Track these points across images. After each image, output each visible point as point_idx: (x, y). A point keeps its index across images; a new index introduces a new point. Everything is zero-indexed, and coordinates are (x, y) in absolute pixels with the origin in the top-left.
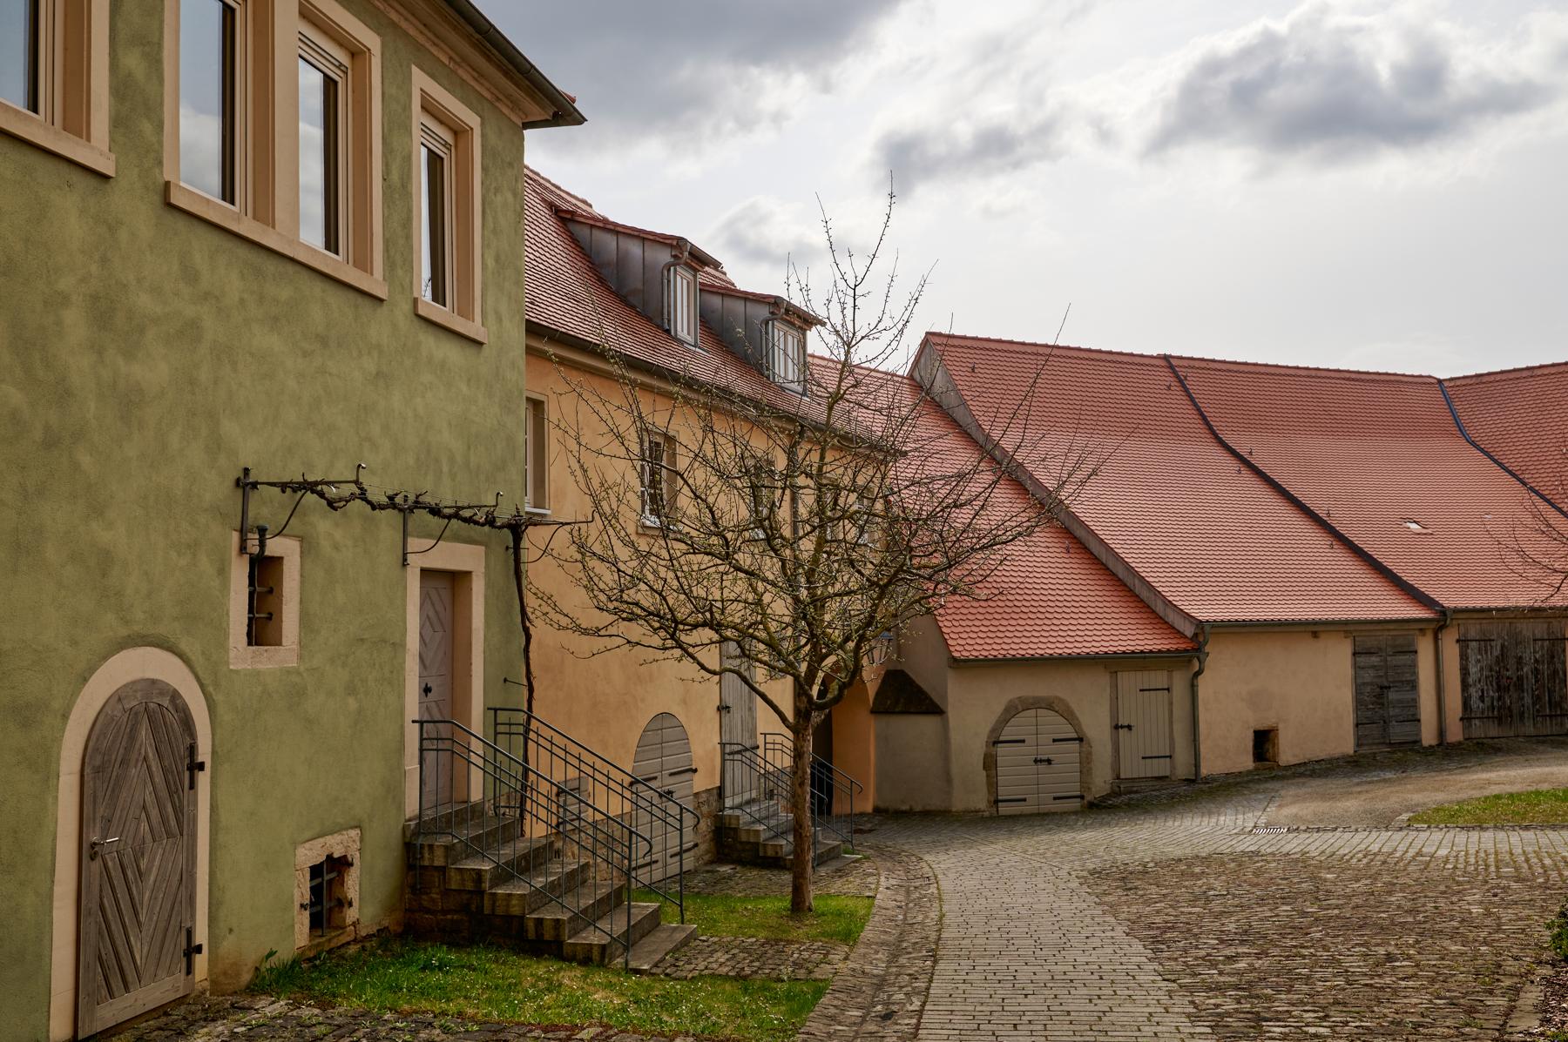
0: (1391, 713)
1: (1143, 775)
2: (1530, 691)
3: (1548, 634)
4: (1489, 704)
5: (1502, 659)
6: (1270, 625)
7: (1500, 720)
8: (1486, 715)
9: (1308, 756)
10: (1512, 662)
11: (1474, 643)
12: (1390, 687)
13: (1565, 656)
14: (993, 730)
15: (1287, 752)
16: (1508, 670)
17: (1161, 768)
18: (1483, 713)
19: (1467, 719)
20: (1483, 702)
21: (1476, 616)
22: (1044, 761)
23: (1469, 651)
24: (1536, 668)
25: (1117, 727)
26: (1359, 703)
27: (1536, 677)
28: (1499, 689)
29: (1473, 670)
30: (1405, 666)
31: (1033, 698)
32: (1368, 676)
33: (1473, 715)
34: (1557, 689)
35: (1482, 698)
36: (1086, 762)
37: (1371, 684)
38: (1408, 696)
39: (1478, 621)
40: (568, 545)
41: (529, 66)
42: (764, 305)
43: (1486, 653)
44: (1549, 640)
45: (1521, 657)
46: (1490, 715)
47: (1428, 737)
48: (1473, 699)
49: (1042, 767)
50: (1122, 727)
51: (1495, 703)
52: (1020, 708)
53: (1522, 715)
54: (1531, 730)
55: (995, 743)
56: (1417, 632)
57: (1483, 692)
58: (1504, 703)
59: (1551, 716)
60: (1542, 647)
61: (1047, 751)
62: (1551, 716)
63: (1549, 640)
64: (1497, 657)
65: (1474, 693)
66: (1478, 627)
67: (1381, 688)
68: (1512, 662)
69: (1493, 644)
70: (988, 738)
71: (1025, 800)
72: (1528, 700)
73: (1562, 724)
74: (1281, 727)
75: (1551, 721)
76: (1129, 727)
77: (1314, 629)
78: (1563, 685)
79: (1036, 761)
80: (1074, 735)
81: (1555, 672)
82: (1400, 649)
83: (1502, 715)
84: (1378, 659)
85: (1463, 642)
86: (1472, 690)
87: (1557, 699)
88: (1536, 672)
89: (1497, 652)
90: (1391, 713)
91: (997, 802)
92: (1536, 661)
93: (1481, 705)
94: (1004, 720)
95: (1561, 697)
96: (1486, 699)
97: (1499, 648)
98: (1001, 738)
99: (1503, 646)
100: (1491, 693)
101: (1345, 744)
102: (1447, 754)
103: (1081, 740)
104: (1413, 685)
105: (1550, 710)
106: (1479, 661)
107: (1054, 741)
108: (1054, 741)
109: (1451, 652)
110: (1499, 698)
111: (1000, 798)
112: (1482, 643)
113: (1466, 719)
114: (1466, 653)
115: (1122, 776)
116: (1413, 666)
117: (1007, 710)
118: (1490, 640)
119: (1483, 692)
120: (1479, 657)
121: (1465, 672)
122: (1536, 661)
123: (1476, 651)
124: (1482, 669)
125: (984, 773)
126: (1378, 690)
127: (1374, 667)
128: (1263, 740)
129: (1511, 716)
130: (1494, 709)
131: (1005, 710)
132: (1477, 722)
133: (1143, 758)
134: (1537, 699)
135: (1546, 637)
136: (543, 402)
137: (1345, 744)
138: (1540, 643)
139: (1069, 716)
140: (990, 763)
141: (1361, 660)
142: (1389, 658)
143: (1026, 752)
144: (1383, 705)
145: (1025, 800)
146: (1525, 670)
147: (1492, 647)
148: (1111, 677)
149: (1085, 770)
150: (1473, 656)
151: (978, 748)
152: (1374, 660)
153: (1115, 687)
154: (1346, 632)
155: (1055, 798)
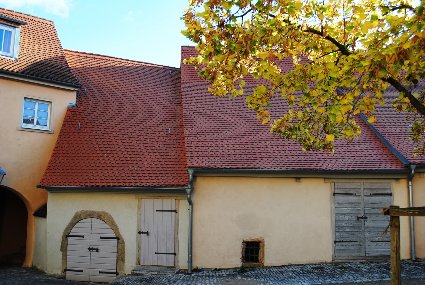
1: (152, 265)
14: (67, 229)
17: (167, 261)
22: (94, 249)
25: (140, 233)
40: (338, 116)
42: (415, 220)
49: (94, 253)
50: (143, 233)
52: (82, 217)
61: (97, 243)
70: (64, 233)
71: (82, 271)
76: (147, 233)
79: (90, 249)
82: (375, 192)
91: (66, 270)
94: (72, 224)
103: (118, 239)
107: (101, 238)
108: (101, 238)
111: (68, 268)
115: (142, 263)
117: (75, 218)
125: (61, 253)
131: (74, 217)
139: (113, 225)
140: (64, 248)
143: (86, 243)
145: (82, 271)
148: (138, 201)
149: (120, 257)
151: (59, 237)
153: (139, 208)
155: (100, 272)
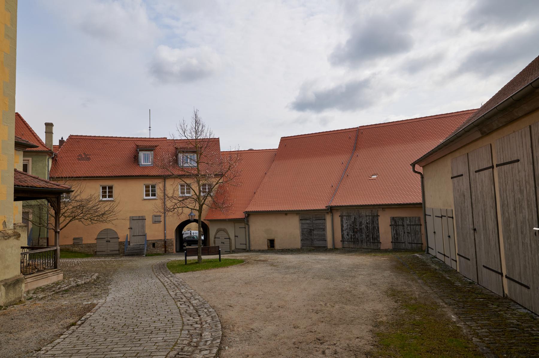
0: (314, 238)
2: (365, 233)
3: (371, 214)
4: (350, 237)
5: (354, 222)
6: (269, 212)
7: (354, 242)
8: (349, 240)
9: (284, 248)
10: (358, 224)
11: (345, 217)
12: (314, 230)
13: (378, 222)
15: (277, 246)
16: (357, 226)
18: (348, 239)
19: (343, 241)
20: (348, 236)
21: (349, 208)
23: (343, 219)
24: (367, 226)
25: (235, 236)
26: (303, 234)
27: (367, 229)
28: (354, 232)
29: (345, 225)
30: (320, 223)
31: (326, 226)
32: (305, 226)
33: (345, 240)
34: (375, 233)
35: (348, 235)
36: (230, 243)
37: (307, 228)
38: (323, 233)
39: (347, 210)
41: (428, 154)
43: (349, 220)
44: (372, 216)
45: (361, 222)
46: (351, 240)
47: (330, 245)
48: (345, 235)
51: (352, 237)
53: (362, 241)
54: (365, 247)
55: (215, 238)
56: (326, 213)
57: (348, 233)
58: (355, 237)
59: (373, 243)
60: (369, 218)
62: (373, 243)
63: (372, 216)
64: (353, 221)
65: (345, 233)
66: (346, 211)
67: (310, 230)
68: (358, 224)
69: (352, 217)
72: (364, 236)
73: (377, 246)
74: (276, 239)
75: (373, 245)
77: (286, 213)
78: (377, 232)
80: (228, 237)
81: (374, 227)
83: (355, 241)
84: (309, 221)
85: (341, 216)
86: (345, 232)
87: (375, 236)
88: (367, 227)
89: (353, 220)
90: (314, 238)
92: (367, 223)
93: (348, 237)
94: (216, 233)
95: (377, 236)
96: (349, 235)
97: (353, 219)
98: (216, 237)
99: (355, 218)
100: (351, 233)
101: (298, 245)
102: (334, 250)
103: (229, 238)
104: (324, 229)
105: (373, 240)
106: (347, 223)
109: (337, 220)
110: (354, 235)
112: (348, 217)
113: (343, 241)
114: (342, 220)
116: (324, 224)
118: (350, 216)
119: (348, 233)
120: (347, 221)
121: (342, 226)
122: (367, 223)
123: (345, 219)
124: (348, 225)
126: (309, 230)
127: (307, 224)
128: (272, 243)
129: (358, 241)
130: (352, 238)
132: (346, 242)
133: (240, 244)
134: (368, 236)
135: (370, 215)
136: (27, 164)
137: (298, 245)
138: (368, 217)
141: (304, 222)
142: (314, 221)
144: (311, 235)
146: (363, 226)
147: (351, 218)
150: (345, 221)
152: (308, 222)
154: (297, 213)
